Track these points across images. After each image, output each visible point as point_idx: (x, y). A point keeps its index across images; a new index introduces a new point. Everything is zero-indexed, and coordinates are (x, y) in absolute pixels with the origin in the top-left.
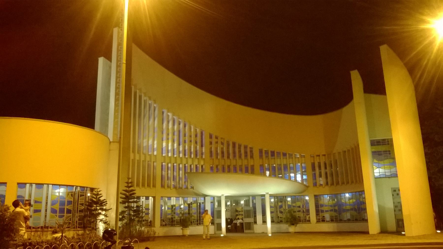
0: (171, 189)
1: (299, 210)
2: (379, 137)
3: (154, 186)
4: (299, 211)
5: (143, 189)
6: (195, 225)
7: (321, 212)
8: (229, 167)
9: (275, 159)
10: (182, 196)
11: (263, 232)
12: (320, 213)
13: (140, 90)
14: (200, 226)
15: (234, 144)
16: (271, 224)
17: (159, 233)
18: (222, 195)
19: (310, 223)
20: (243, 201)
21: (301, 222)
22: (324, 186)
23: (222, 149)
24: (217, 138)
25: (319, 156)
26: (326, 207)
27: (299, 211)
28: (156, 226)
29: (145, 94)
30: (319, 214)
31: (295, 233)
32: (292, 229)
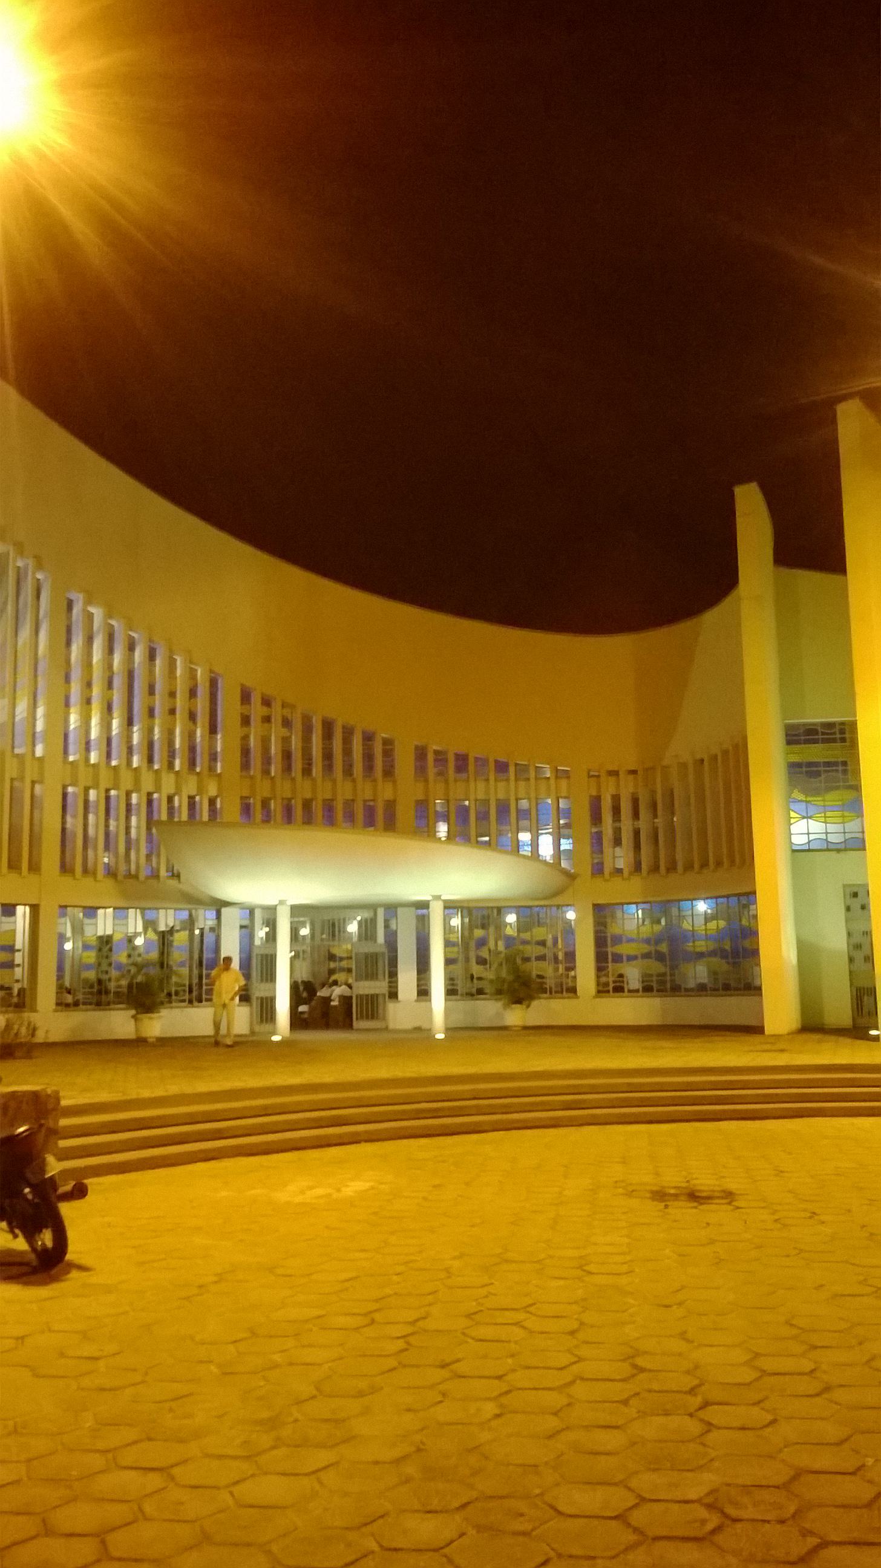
3: (34, 867)
8: (307, 805)
15: (328, 727)
21: (546, 993)
32: (515, 1016)
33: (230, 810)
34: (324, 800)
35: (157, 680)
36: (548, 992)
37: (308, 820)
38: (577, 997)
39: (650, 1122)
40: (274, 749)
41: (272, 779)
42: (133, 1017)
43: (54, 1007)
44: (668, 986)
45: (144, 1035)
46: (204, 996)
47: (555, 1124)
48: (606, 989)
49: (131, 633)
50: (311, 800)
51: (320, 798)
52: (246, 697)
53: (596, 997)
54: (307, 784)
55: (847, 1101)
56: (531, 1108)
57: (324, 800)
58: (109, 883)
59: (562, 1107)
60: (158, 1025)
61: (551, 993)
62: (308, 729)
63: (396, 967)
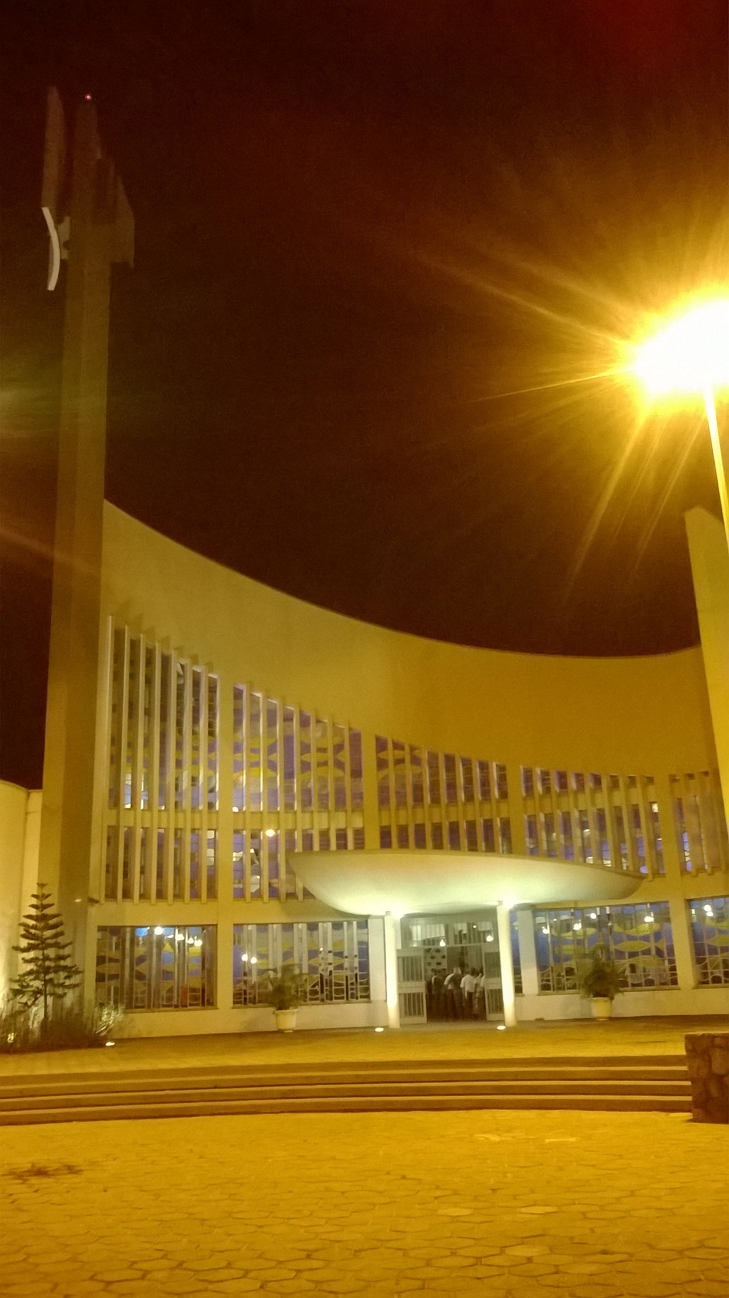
0: (264, 903)
1: (646, 948)
2: (254, 747)
3: (212, 893)
4: (647, 952)
5: (195, 904)
6: (317, 1002)
7: (710, 954)
8: (403, 830)
9: (312, 812)
10: (347, 919)
11: (541, 1020)
12: (707, 956)
13: (166, 641)
14: (332, 1004)
15: (450, 761)
16: (515, 996)
17: (139, 1031)
18: (386, 912)
19: (369, 1002)
20: (578, 923)
21: (550, 989)
22: (650, 878)
23: (337, 780)
24: (397, 746)
25: (691, 776)
26: (113, 964)
27: (647, 952)
28: (219, 1004)
29: (180, 650)
30: (704, 959)
31: (611, 1019)
32: (599, 1008)
33: (373, 838)
34: (338, 830)
35: (295, 732)
36: (552, 989)
37: (421, 844)
38: (523, 996)
39: (352, 1111)
40: (331, 789)
41: (295, 813)
42: (274, 1013)
43: (232, 1005)
44: (710, 979)
45: (281, 1027)
46: (334, 995)
47: (55, 1120)
48: (706, 980)
49: (269, 700)
50: (345, 830)
51: (300, 827)
52: (381, 745)
53: (696, 987)
54: (290, 816)
55: (579, 1094)
56: (228, 1098)
57: (303, 831)
58: (274, 903)
59: (279, 1096)
60: (291, 1019)
61: (554, 990)
62: (434, 767)
63: (519, 965)
